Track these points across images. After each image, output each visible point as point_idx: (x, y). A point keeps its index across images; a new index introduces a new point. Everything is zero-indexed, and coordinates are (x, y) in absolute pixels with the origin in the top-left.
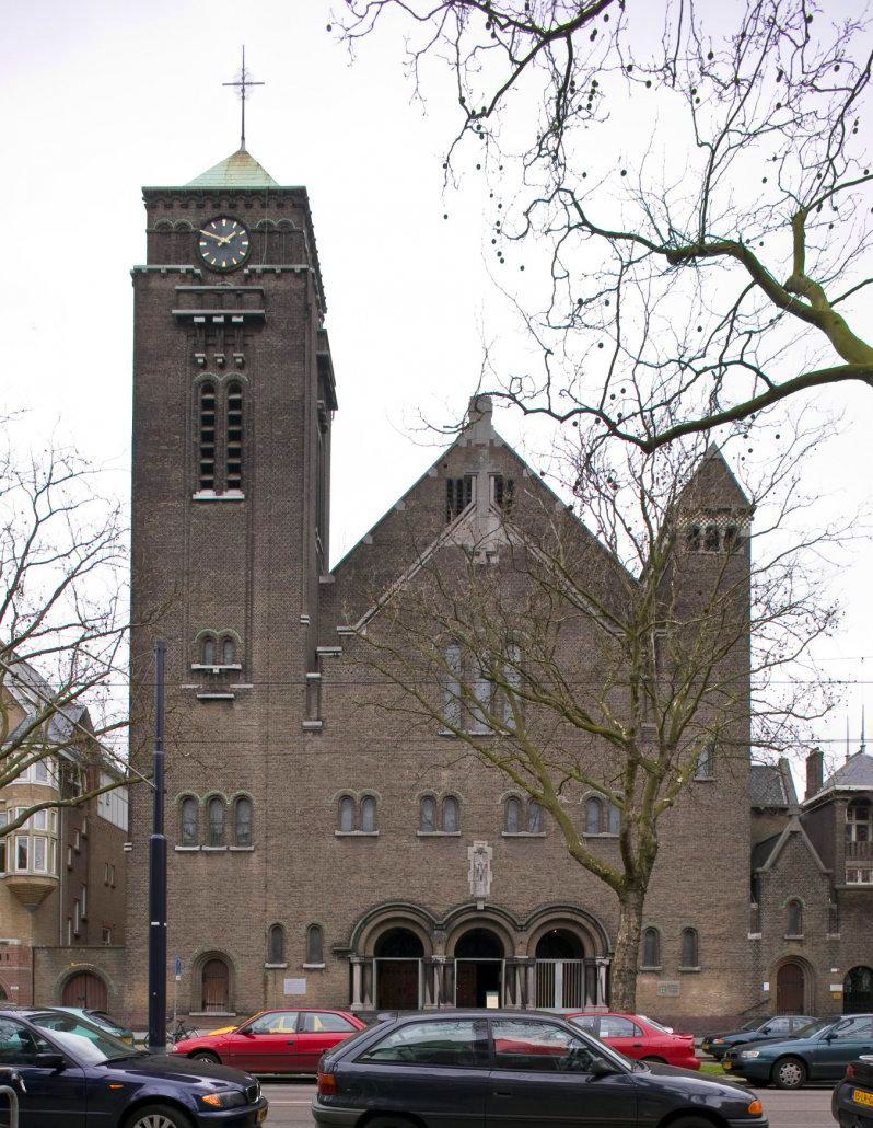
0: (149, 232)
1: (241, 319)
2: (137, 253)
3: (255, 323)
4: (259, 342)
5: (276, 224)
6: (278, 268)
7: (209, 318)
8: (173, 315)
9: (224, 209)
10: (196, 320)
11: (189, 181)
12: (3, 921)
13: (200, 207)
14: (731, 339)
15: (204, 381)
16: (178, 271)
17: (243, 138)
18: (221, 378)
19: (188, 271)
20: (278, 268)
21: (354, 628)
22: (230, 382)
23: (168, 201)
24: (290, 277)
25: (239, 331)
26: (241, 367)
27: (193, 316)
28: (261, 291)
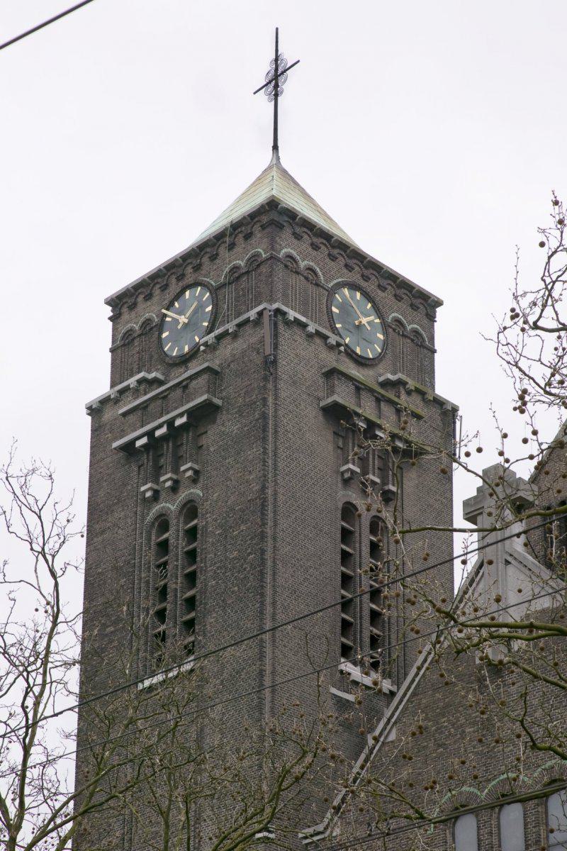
0: (112, 351)
1: (184, 419)
2: (97, 380)
3: (204, 415)
4: (212, 437)
5: (409, 328)
6: (231, 327)
7: (150, 434)
8: (115, 449)
9: (189, 279)
10: (139, 443)
11: (197, 236)
12: (564, 661)
13: (165, 288)
14: (24, 719)
15: (156, 519)
16: (247, 321)
17: (275, 147)
18: (171, 506)
19: (140, 382)
20: (231, 327)
21: (320, 828)
22: (185, 505)
23: (131, 301)
24: (248, 329)
25: (188, 433)
26: (194, 481)
27: (133, 441)
28: (208, 369)
